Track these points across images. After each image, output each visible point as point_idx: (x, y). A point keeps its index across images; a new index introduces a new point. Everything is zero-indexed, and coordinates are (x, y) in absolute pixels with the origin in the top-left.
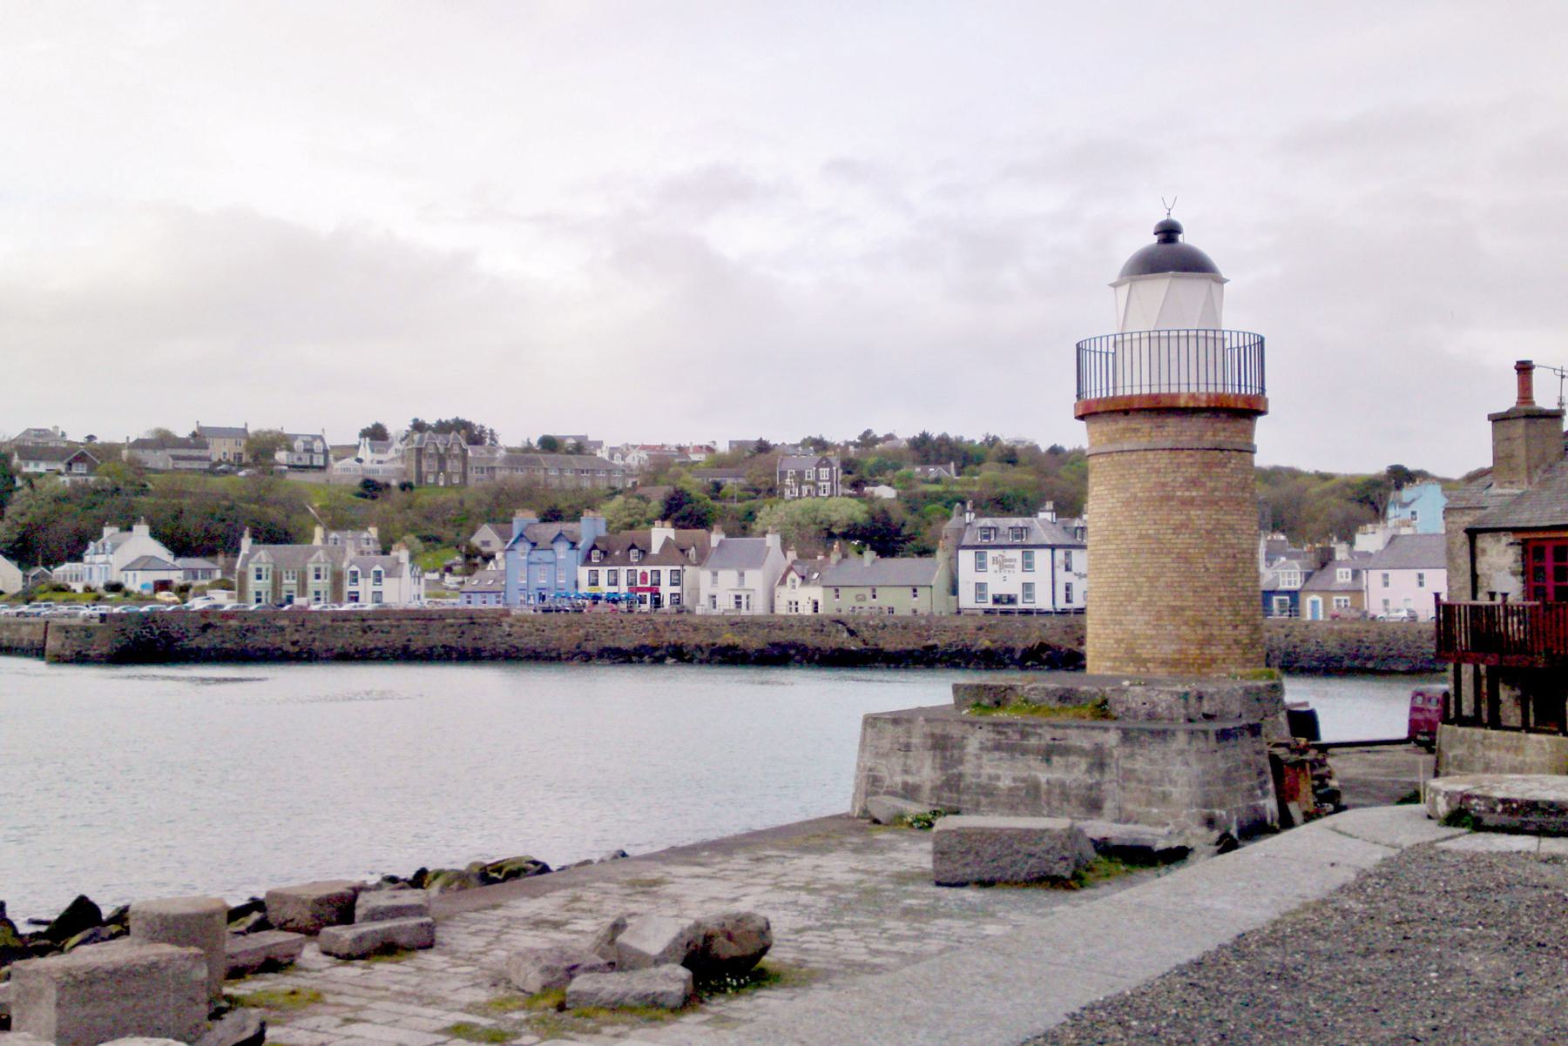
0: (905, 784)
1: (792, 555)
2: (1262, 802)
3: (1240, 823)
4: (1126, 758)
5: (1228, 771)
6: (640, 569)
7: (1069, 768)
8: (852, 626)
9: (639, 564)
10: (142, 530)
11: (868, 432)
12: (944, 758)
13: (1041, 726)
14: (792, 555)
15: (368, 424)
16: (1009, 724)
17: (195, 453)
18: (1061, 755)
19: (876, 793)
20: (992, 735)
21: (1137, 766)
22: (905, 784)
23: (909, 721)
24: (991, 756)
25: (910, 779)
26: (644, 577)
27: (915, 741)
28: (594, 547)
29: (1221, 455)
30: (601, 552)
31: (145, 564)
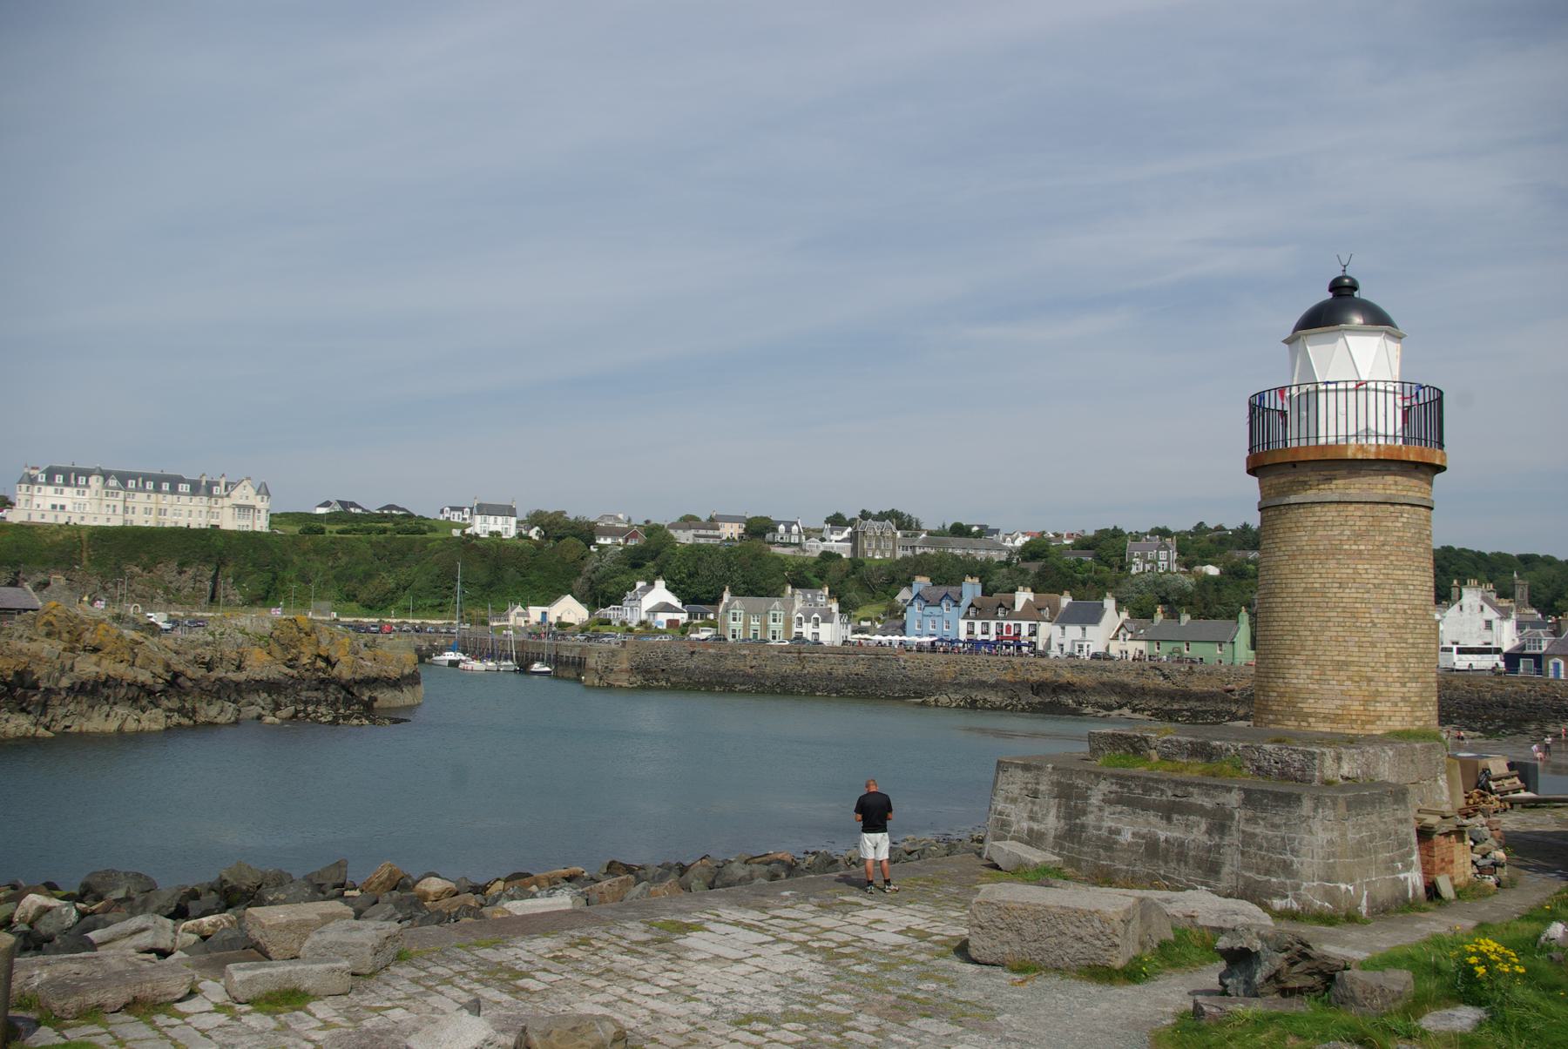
0: (1031, 830)
1: (1124, 615)
2: (1402, 876)
3: (1371, 898)
4: (1247, 820)
5: (1360, 842)
6: (1005, 623)
7: (1188, 827)
8: (1166, 672)
9: (1005, 618)
10: (660, 584)
11: (1201, 523)
12: (1068, 807)
13: (1163, 782)
14: (1124, 615)
15: (830, 514)
16: (1132, 778)
17: (710, 533)
18: (1180, 813)
19: (1003, 838)
20: (1114, 788)
21: (1258, 831)
22: (1031, 830)
23: (1039, 768)
24: (1112, 809)
25: (1035, 826)
26: (1008, 627)
27: (1042, 788)
28: (972, 605)
29: (1391, 509)
30: (978, 611)
31: (666, 608)
